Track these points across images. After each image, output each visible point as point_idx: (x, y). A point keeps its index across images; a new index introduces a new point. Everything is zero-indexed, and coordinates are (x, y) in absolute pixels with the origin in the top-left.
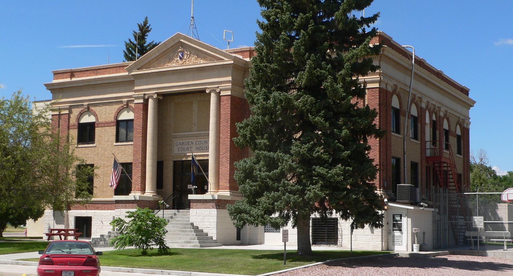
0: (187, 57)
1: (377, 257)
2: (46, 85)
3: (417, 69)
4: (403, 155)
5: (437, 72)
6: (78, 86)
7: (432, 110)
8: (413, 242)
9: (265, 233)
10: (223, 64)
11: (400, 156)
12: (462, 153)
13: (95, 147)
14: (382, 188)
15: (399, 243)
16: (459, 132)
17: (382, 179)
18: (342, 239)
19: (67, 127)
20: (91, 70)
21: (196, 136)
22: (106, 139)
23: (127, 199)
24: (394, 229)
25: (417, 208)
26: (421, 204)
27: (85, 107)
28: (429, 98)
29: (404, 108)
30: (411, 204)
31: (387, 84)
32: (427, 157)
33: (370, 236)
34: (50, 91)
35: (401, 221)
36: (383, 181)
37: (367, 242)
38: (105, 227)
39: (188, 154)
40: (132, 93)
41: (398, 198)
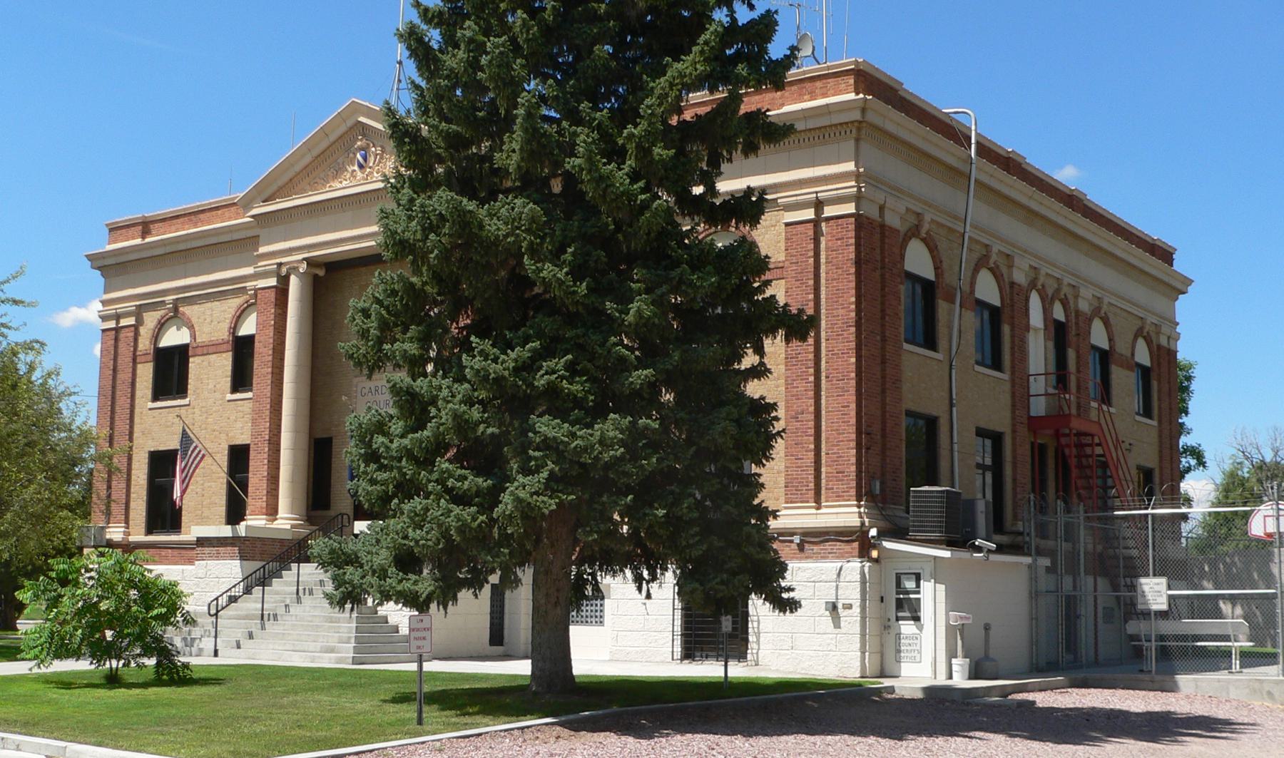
0: (375, 161)
1: (806, 698)
2: (90, 257)
3: (983, 171)
4: (946, 408)
5: (1068, 192)
7: (1050, 292)
8: (951, 654)
11: (935, 407)
12: (1156, 412)
13: (189, 405)
14: (864, 499)
15: (913, 654)
16: (1143, 356)
17: (867, 471)
18: (759, 644)
19: (130, 359)
20: (185, 215)
22: (210, 387)
23: (220, 536)
24: (900, 614)
25: (964, 555)
26: (977, 543)
27: (168, 306)
28: (1036, 256)
29: (950, 278)
30: (950, 544)
31: (882, 208)
32: (1030, 418)
33: (831, 636)
34: (98, 272)
35: (918, 593)
36: (871, 478)
37: (821, 653)
41: (914, 526)
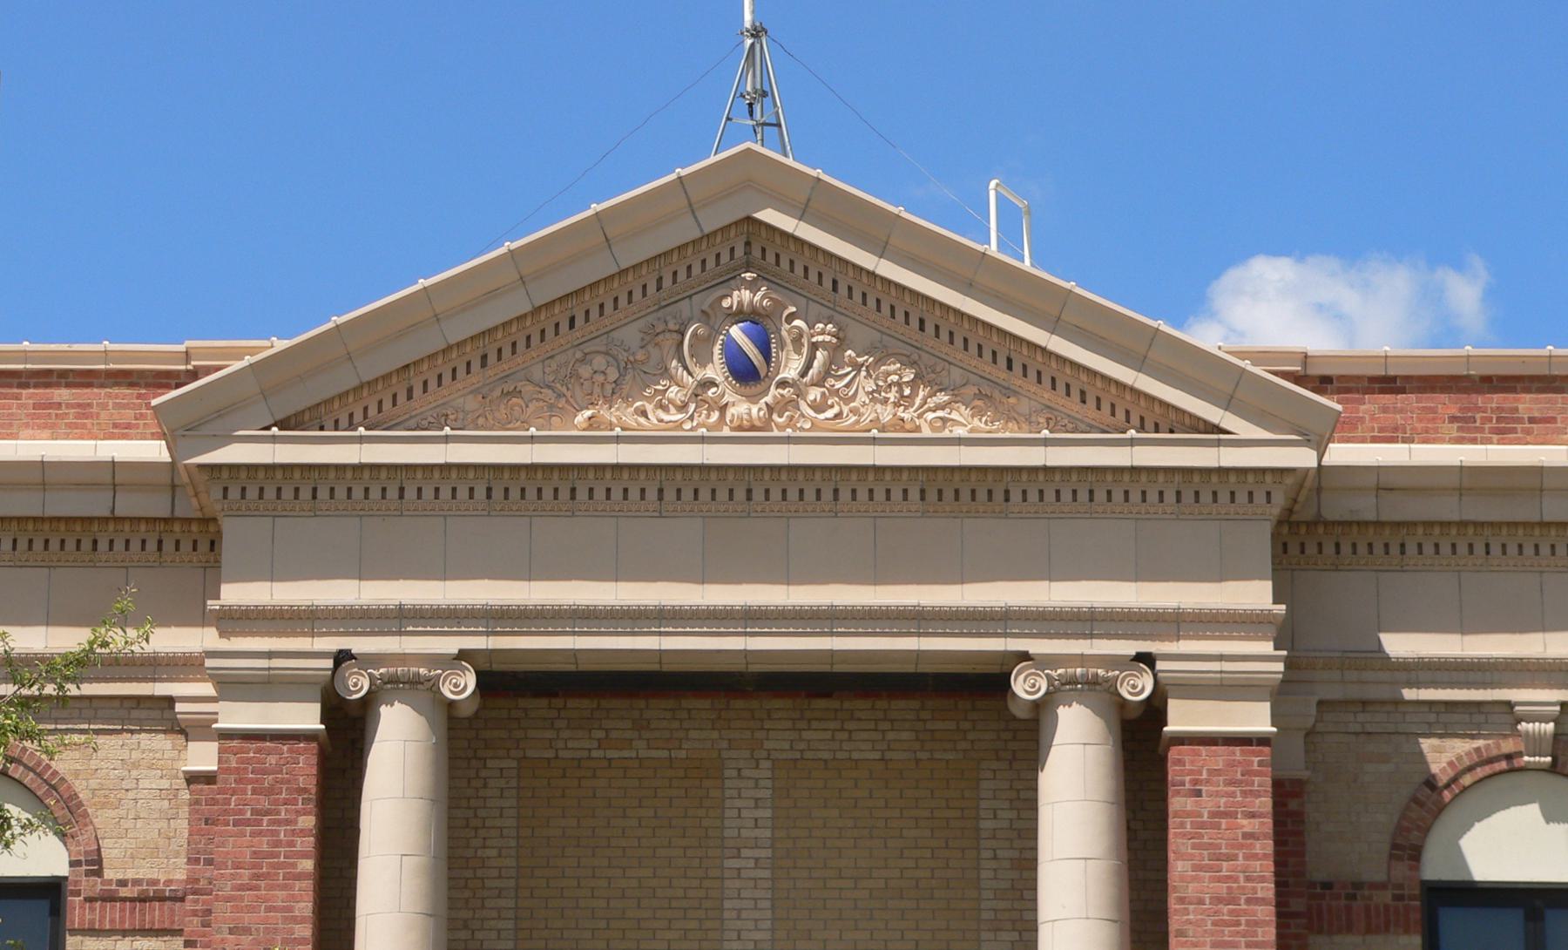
40: (197, 631)
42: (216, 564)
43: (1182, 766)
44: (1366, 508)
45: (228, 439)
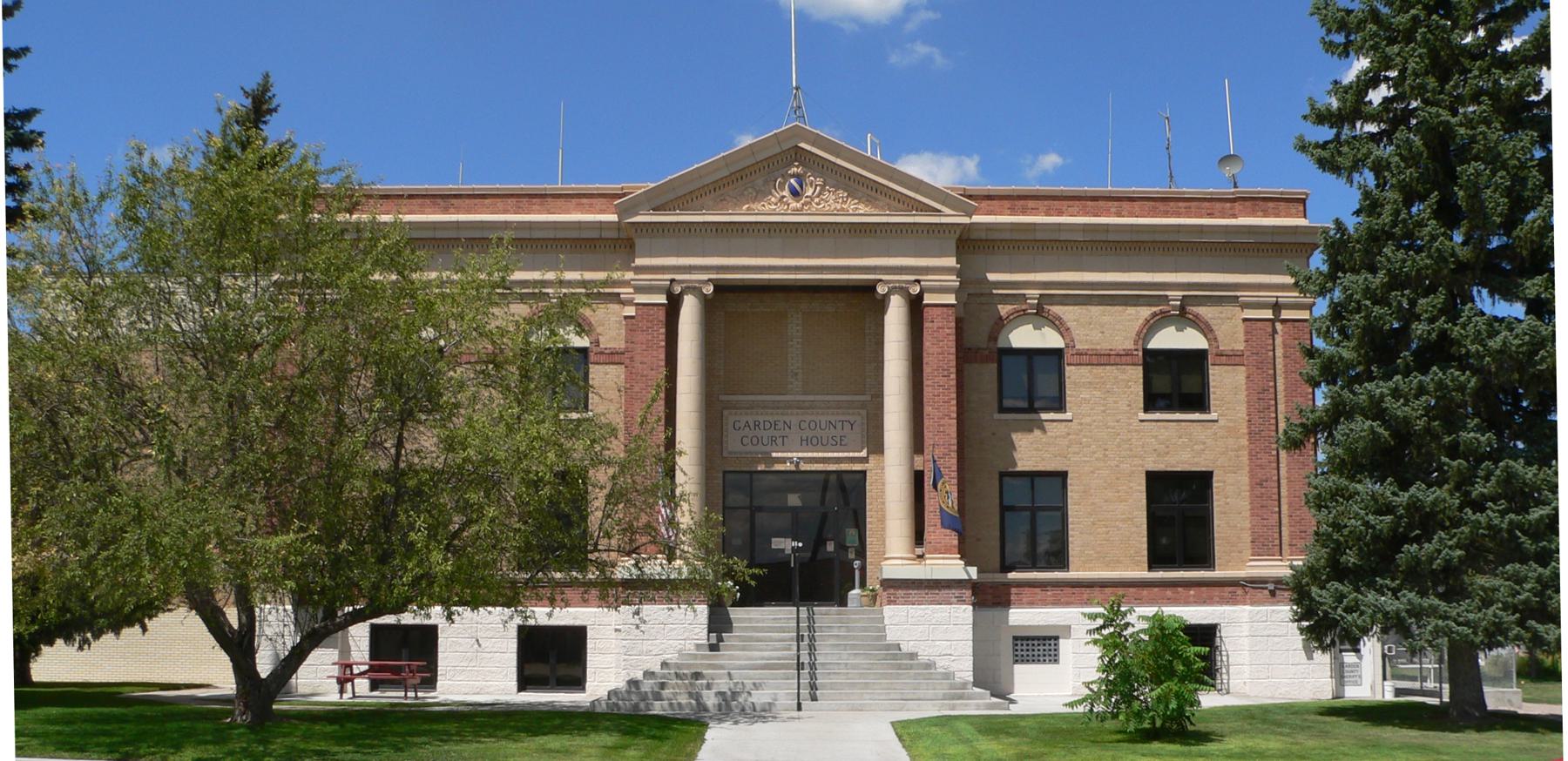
6: (434, 239)
9: (1017, 667)
10: (702, 220)
21: (799, 406)
24: (1342, 647)
38: (489, 655)
39: (774, 455)
42: (634, 252)
43: (928, 313)
44: (983, 236)
45: (637, 214)
